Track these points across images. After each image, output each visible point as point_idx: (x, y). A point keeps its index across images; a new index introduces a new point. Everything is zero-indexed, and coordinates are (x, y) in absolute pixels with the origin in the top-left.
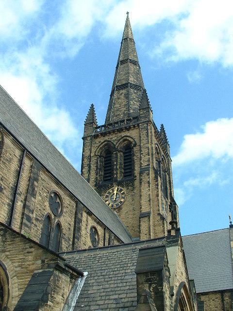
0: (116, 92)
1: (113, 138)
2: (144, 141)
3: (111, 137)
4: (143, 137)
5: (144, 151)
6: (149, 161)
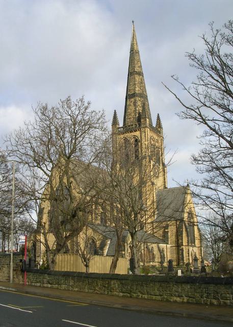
0: (128, 100)
1: (128, 135)
2: (144, 140)
3: (126, 135)
4: (143, 137)
5: (144, 146)
6: (146, 152)
